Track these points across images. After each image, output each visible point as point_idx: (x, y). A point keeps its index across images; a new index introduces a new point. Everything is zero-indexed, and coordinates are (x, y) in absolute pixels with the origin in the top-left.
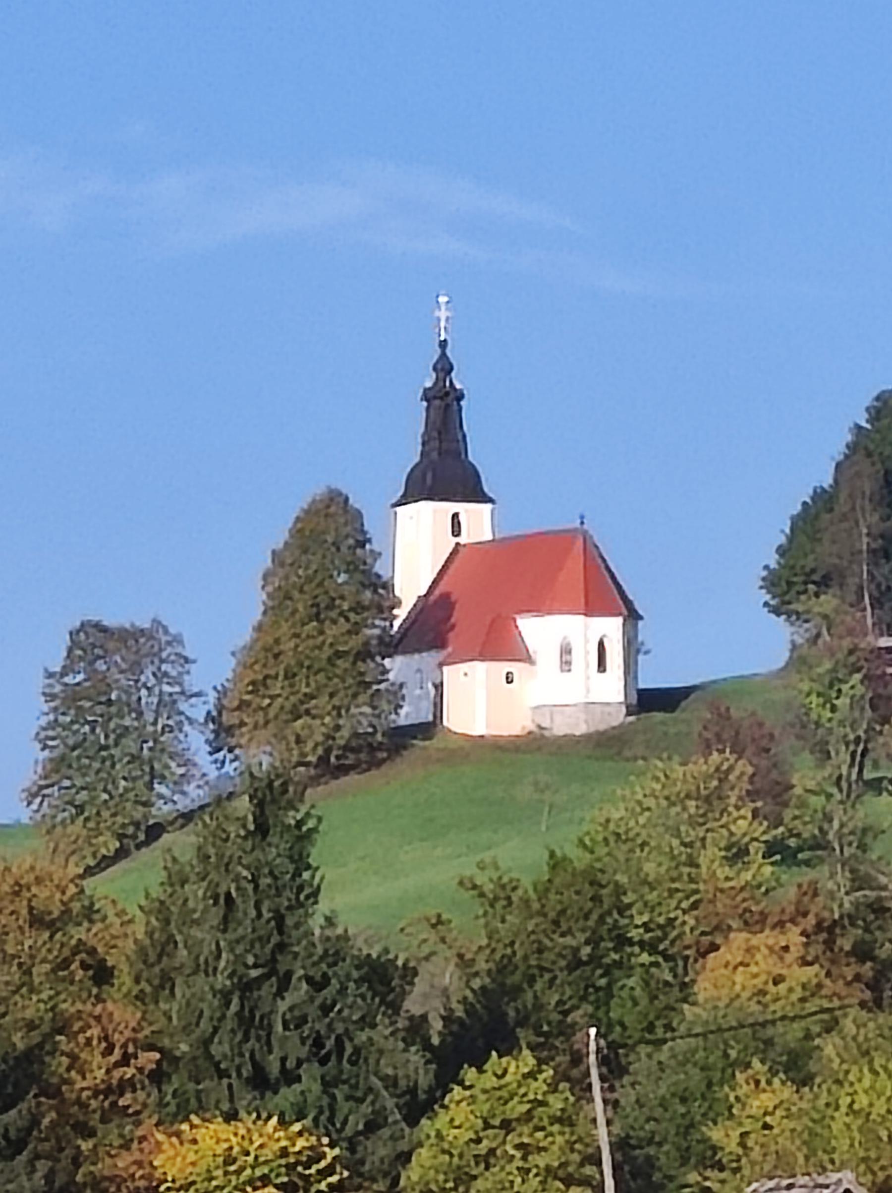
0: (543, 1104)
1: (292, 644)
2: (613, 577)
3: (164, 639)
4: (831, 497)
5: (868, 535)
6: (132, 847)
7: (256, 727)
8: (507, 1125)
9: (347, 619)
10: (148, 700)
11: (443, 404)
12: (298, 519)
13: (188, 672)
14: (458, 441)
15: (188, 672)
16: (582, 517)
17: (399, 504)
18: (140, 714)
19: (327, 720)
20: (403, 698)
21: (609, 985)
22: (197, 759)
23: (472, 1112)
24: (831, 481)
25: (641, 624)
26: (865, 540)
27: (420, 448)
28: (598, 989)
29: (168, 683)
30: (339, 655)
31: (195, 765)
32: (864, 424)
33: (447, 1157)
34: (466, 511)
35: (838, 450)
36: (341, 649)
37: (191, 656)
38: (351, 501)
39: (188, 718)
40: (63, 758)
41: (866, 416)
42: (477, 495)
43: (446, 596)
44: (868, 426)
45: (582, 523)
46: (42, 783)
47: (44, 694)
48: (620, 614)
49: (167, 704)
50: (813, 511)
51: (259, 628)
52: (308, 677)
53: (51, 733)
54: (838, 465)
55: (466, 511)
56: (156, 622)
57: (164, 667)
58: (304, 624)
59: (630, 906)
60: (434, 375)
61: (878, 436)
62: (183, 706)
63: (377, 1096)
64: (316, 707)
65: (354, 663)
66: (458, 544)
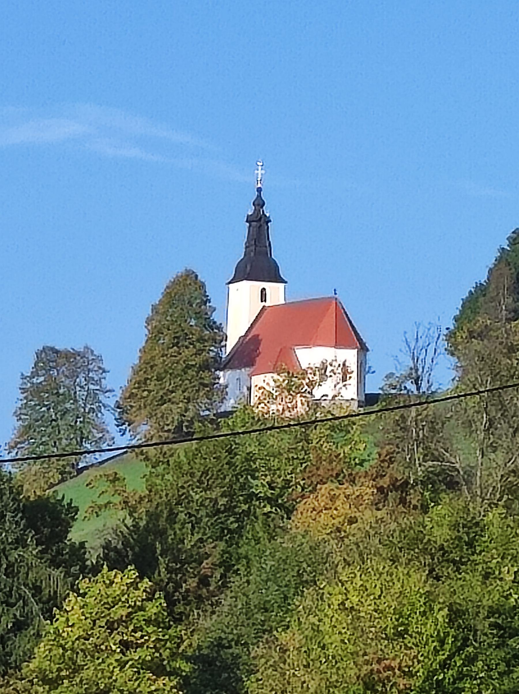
0: (142, 609)
1: (161, 360)
2: (350, 322)
3: (91, 358)
4: (485, 289)
5: (506, 310)
6: (68, 478)
7: (140, 408)
8: (111, 627)
9: (195, 347)
10: (81, 394)
11: (258, 225)
12: (168, 287)
13: (105, 378)
14: (266, 247)
15: (105, 378)
16: (335, 290)
17: (230, 283)
18: (76, 401)
19: (181, 405)
20: (227, 394)
21: (240, 528)
22: (109, 428)
23: (83, 614)
24: (486, 278)
25: (368, 353)
26: (504, 312)
27: (244, 250)
28: (230, 531)
29: (92, 384)
30: (188, 367)
31: (108, 432)
32: (506, 247)
33: (61, 651)
34: (270, 287)
35: (491, 262)
36: (190, 363)
37: (107, 369)
38: (199, 277)
39: (103, 405)
40: (30, 427)
41: (507, 242)
42: (277, 278)
43: (256, 336)
44: (508, 249)
45: (335, 294)
46: (18, 440)
47: (20, 389)
48: (357, 348)
49: (92, 395)
50: (475, 296)
51: (143, 351)
52: (170, 380)
53: (24, 411)
54: (491, 269)
55: (270, 287)
56: (86, 347)
57: (91, 375)
58: (169, 348)
59: (257, 470)
60: (253, 208)
61: (514, 254)
62: (101, 397)
63: (25, 604)
64: (174, 397)
65: (197, 373)
66: (264, 306)
